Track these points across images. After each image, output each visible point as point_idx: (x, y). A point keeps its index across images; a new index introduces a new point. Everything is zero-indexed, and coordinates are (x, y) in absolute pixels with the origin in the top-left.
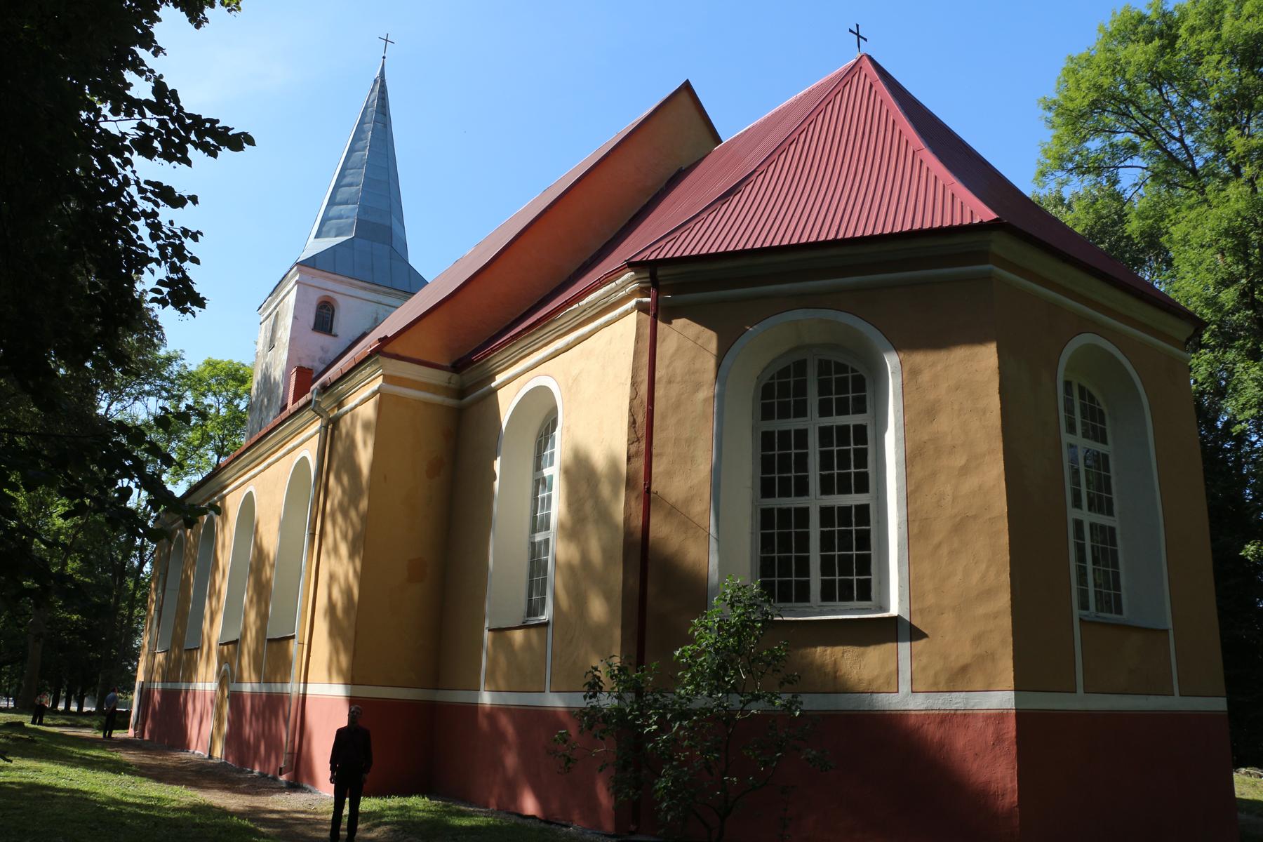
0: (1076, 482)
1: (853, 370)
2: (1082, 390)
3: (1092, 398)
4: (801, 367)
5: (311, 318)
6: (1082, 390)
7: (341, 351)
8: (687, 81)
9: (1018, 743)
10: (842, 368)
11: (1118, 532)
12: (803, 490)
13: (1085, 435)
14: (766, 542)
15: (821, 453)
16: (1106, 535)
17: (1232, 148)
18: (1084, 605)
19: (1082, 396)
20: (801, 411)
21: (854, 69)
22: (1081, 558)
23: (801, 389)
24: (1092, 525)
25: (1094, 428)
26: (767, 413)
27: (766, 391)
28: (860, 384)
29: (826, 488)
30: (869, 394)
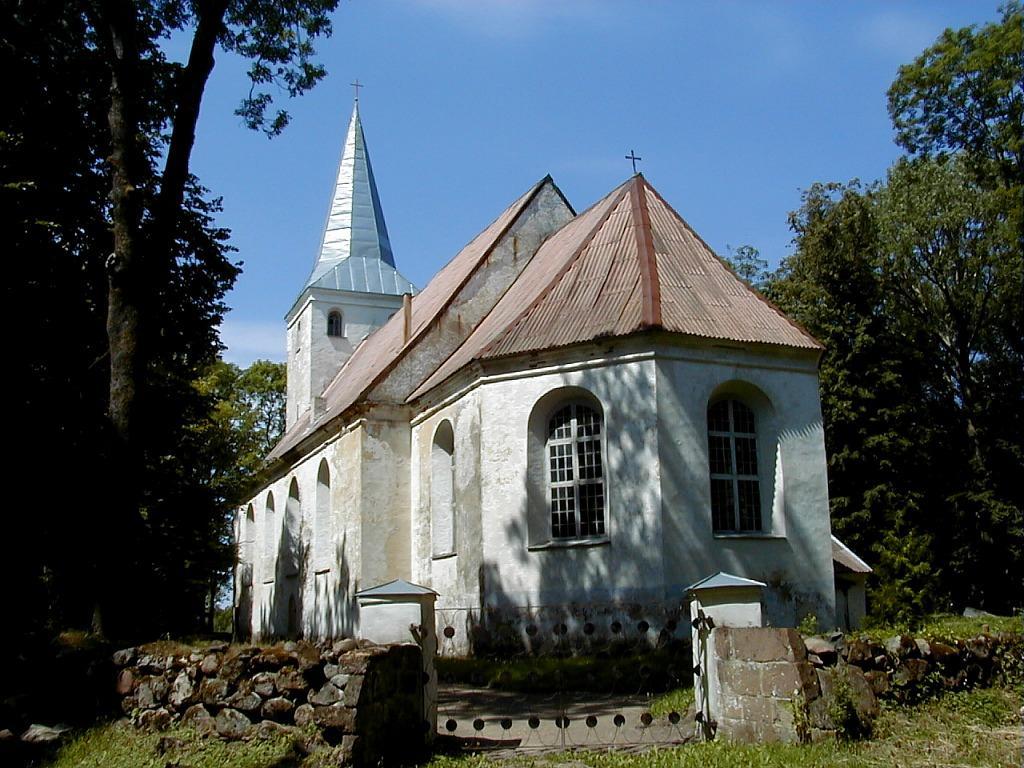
5: (324, 325)
8: (549, 175)
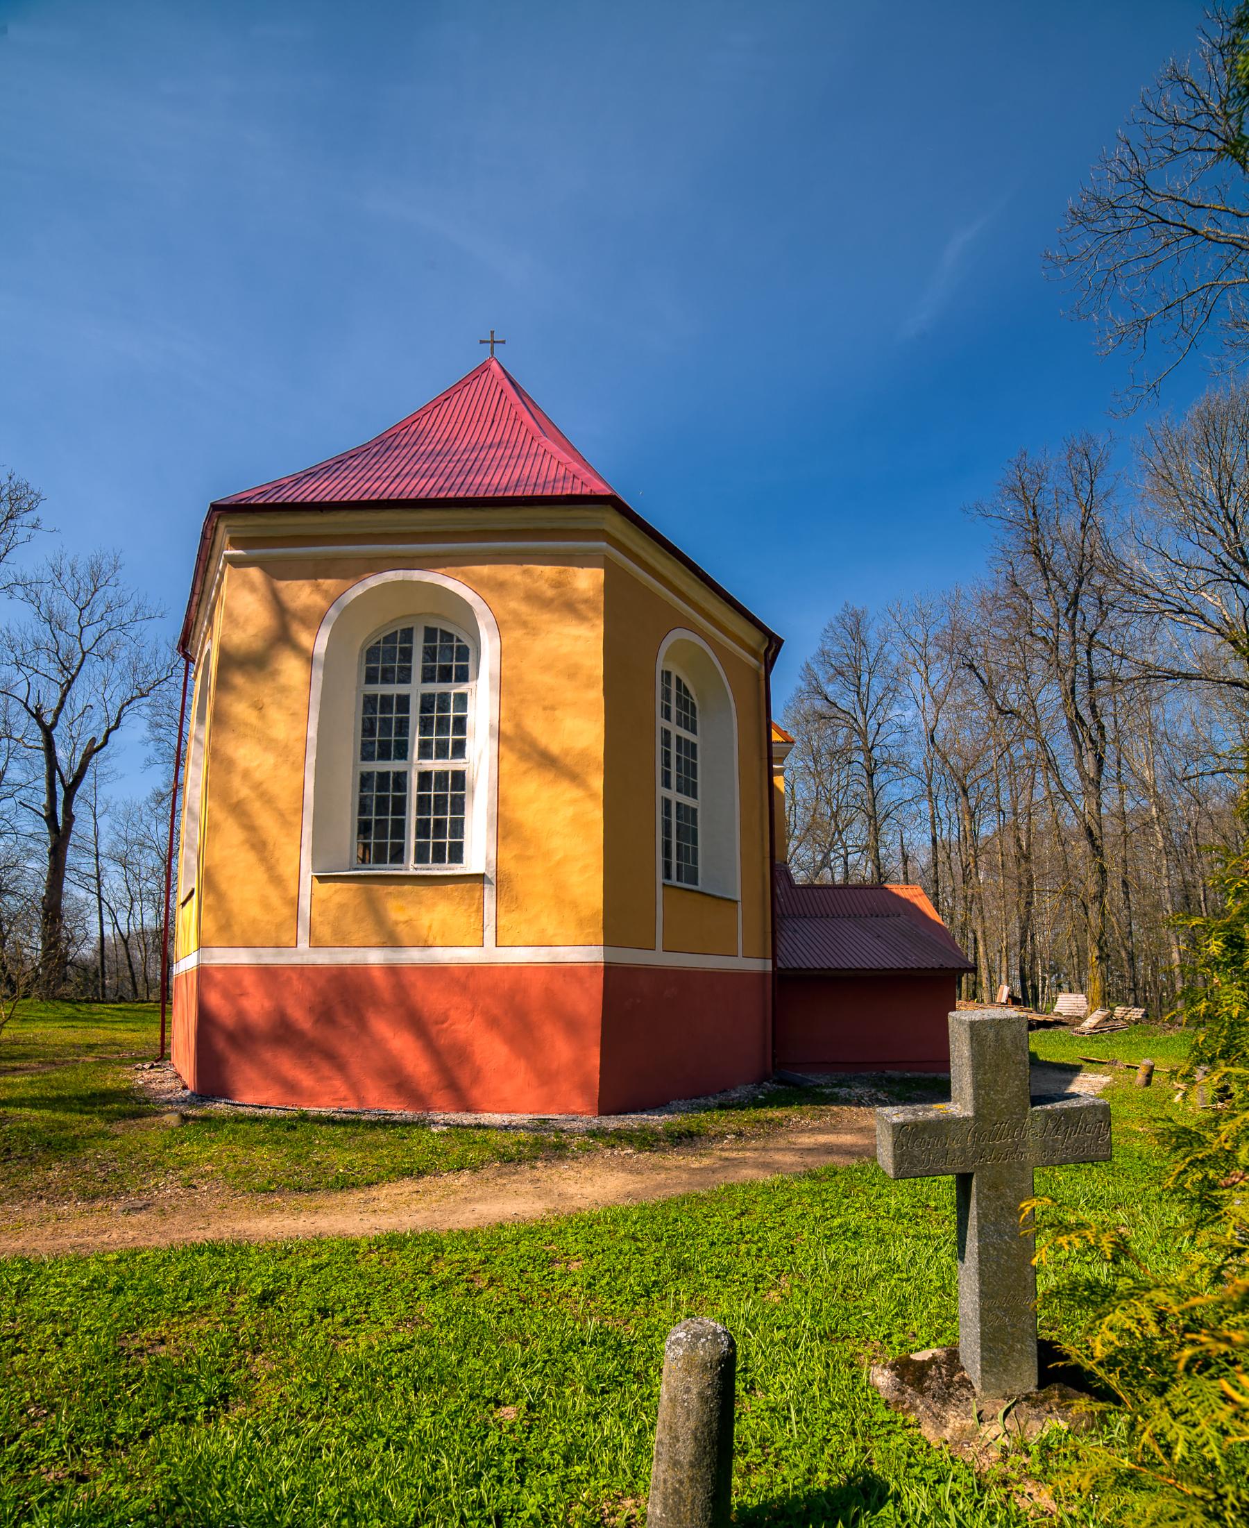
0: (668, 764)
1: (458, 640)
2: (679, 681)
3: (687, 692)
4: (408, 634)
6: (679, 681)
7: (709, 899)
9: (601, 1073)
10: (448, 636)
11: (699, 814)
12: (402, 753)
13: (679, 724)
14: (363, 808)
15: (408, 712)
16: (687, 814)
17: (250, 1398)
18: (668, 875)
19: (678, 688)
20: (405, 678)
21: (484, 368)
22: (667, 832)
23: (407, 655)
24: (678, 804)
25: (686, 718)
26: (371, 678)
27: (371, 654)
28: (463, 653)
29: (425, 753)
30: (471, 664)
